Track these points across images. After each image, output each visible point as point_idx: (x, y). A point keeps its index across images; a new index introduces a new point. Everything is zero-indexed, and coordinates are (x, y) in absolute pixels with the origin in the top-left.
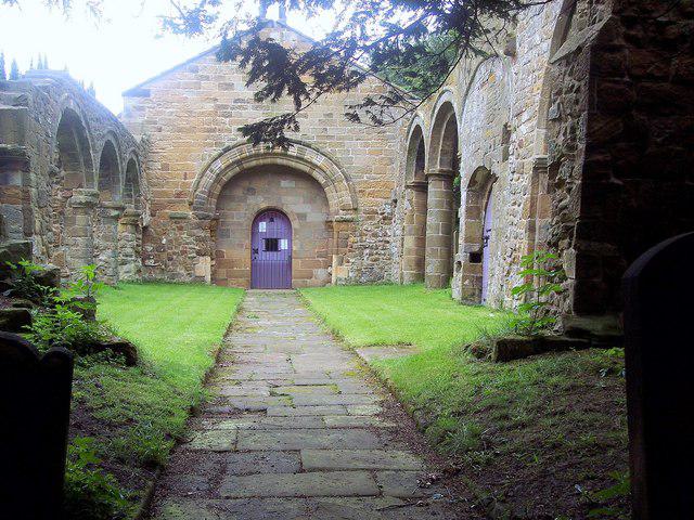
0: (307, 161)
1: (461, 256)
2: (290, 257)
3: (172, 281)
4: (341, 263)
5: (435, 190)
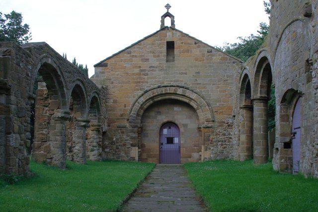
0: (187, 97)
1: (278, 144)
2: (180, 147)
3: (117, 160)
4: (206, 150)
5: (258, 108)
